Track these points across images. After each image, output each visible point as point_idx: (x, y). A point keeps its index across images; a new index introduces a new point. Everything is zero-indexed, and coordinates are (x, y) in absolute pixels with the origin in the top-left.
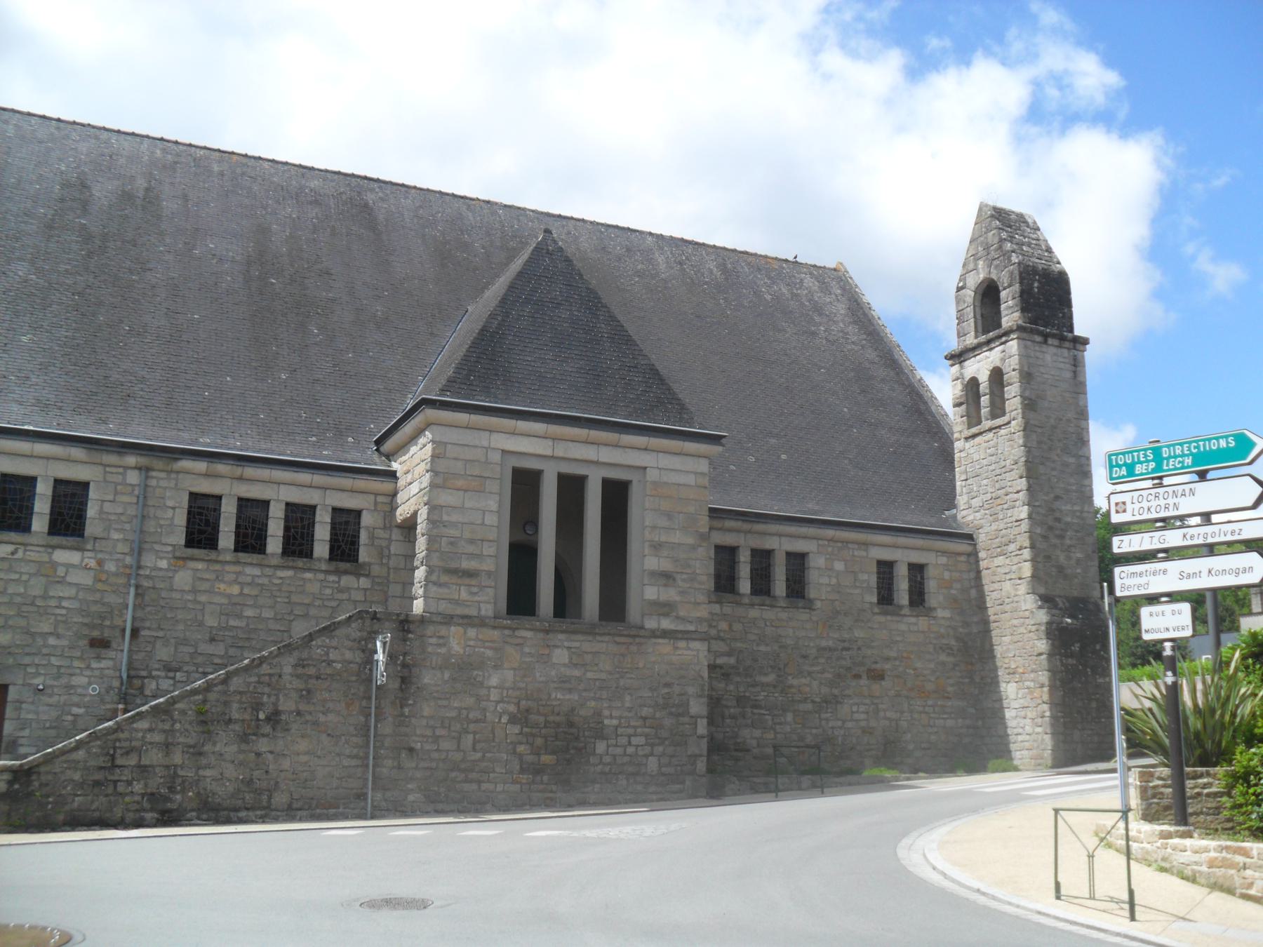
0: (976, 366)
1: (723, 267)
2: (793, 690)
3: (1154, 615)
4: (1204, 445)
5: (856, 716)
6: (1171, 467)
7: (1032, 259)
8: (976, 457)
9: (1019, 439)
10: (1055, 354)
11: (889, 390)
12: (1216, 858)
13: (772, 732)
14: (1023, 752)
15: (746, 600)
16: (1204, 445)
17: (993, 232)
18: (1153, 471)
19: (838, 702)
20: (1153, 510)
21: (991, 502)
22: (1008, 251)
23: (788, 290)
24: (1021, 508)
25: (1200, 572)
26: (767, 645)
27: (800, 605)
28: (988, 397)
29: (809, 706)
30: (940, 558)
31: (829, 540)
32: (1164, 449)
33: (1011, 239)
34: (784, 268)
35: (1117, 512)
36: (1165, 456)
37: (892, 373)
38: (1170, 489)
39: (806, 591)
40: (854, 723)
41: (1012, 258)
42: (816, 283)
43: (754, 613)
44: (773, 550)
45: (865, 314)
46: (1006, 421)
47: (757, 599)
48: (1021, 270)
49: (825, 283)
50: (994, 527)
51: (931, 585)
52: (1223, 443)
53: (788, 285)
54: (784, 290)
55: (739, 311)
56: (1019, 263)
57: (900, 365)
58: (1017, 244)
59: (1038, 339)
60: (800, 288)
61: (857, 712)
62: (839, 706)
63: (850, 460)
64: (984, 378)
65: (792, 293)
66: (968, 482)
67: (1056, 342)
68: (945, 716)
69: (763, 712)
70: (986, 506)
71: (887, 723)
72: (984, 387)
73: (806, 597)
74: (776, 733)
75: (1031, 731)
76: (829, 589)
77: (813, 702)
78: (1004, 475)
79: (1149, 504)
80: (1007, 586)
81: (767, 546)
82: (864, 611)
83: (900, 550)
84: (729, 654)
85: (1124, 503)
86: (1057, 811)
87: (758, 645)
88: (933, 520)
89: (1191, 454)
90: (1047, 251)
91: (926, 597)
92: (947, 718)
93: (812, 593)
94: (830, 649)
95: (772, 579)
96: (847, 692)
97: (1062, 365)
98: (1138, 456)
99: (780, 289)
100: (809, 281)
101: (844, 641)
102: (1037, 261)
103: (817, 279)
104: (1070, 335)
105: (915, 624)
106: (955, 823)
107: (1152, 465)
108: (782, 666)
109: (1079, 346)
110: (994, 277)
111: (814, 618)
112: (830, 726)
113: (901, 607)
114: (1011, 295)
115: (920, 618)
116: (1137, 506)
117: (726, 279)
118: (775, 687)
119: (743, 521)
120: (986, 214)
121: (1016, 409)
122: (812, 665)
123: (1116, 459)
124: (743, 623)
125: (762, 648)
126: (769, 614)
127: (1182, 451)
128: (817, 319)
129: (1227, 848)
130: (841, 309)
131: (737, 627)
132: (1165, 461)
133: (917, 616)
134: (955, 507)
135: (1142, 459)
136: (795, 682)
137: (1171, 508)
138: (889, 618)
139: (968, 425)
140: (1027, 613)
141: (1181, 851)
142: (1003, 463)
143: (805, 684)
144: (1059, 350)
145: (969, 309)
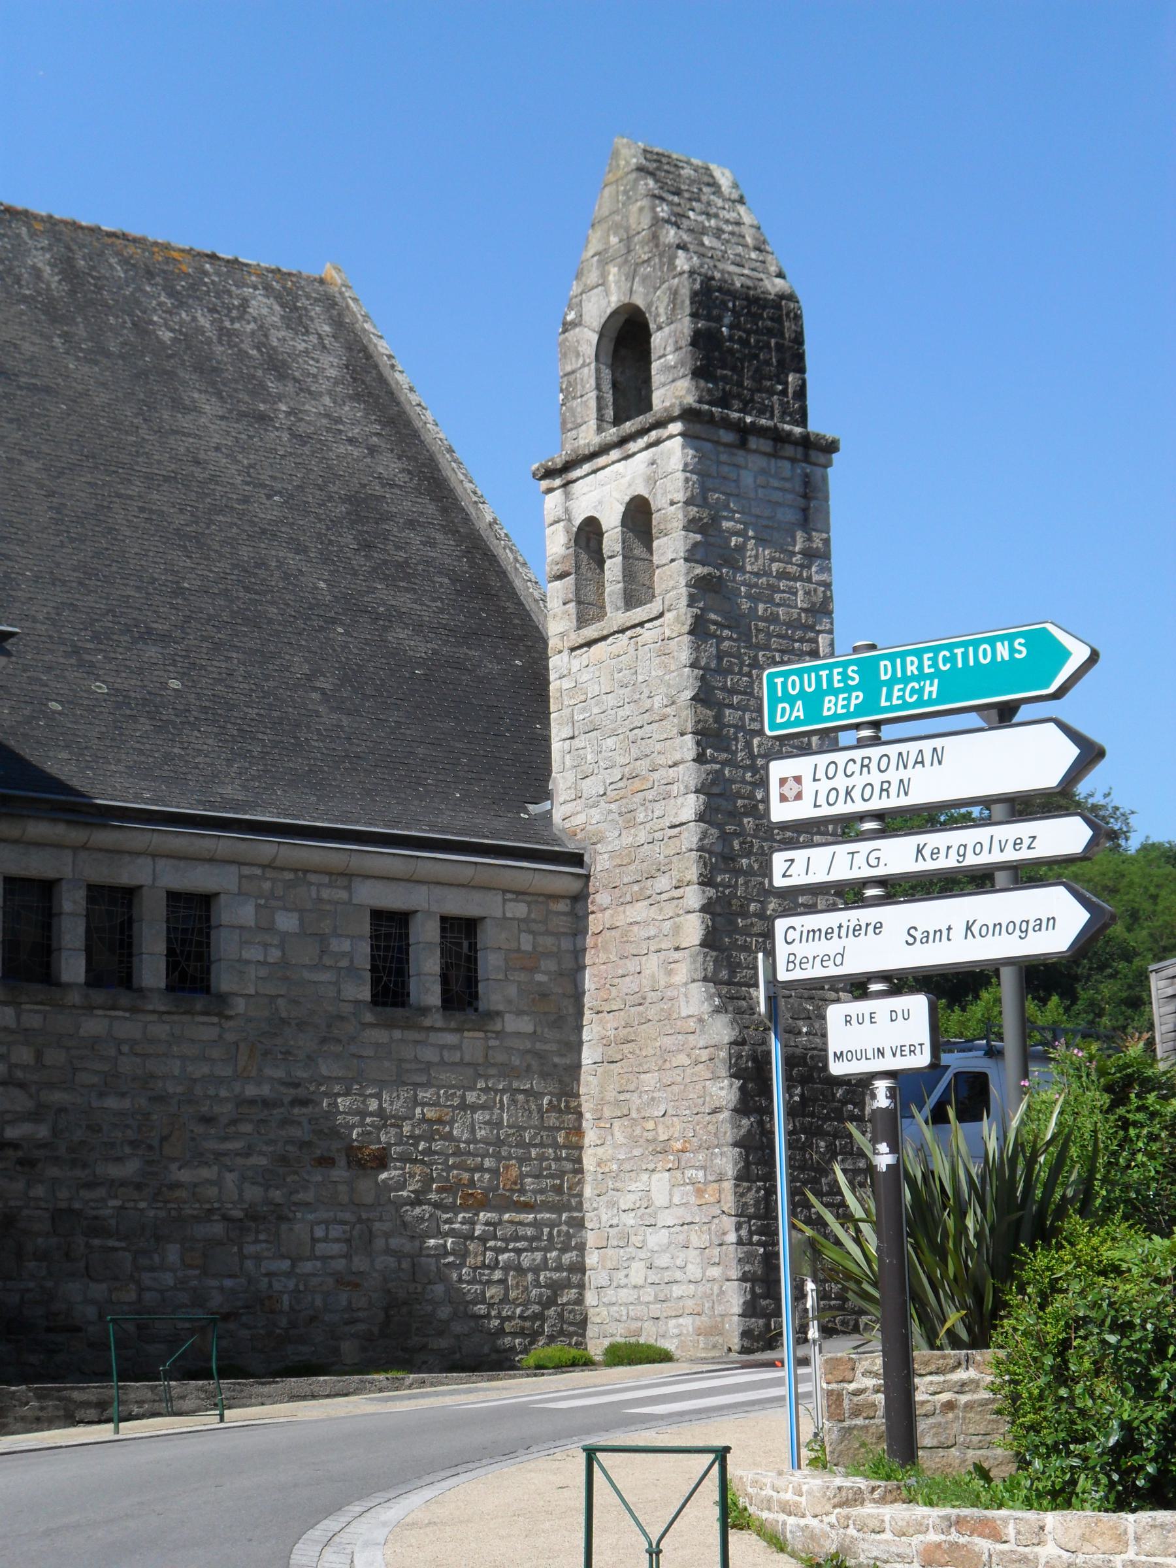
0: (595, 496)
1: (66, 267)
2: (182, 1194)
3: (854, 1022)
4: (965, 655)
5: (321, 1248)
6: (895, 702)
7: (720, 265)
8: (593, 690)
9: (682, 651)
10: (763, 472)
11: (424, 544)
12: (938, 1545)
13: (132, 1286)
14: (681, 1320)
15: (74, 997)
16: (965, 655)
17: (639, 204)
18: (860, 709)
19: (282, 1218)
20: (856, 794)
21: (620, 784)
22: (670, 246)
23: (212, 323)
24: (680, 800)
25: (949, 929)
26: (123, 1095)
27: (199, 1007)
28: (619, 559)
29: (217, 1229)
30: (510, 905)
31: (330, 874)
32: (882, 664)
33: (676, 221)
34: (206, 273)
35: (783, 798)
36: (883, 678)
37: (431, 509)
38: (893, 750)
39: (213, 975)
40: (318, 1264)
41: (678, 262)
42: (277, 308)
43: (93, 1026)
44: (141, 887)
45: (382, 380)
46: (655, 613)
47: (99, 996)
48: (697, 286)
49: (297, 308)
50: (627, 840)
51: (490, 963)
52: (1003, 651)
53: (213, 310)
54: (204, 321)
55: (96, 363)
56: (692, 273)
57: (452, 491)
58: (690, 231)
59: (727, 437)
60: (240, 318)
61: (326, 1240)
62: (284, 1227)
63: (323, 692)
64: (611, 520)
65: (221, 329)
66: (577, 743)
67: (766, 445)
68: (519, 1245)
69: (111, 1243)
70: (611, 795)
71: (391, 1261)
72: (612, 540)
73: (213, 989)
74: (141, 1289)
75: (699, 1276)
76: (263, 972)
77: (226, 1218)
78: (647, 727)
79: (850, 782)
80: (652, 964)
81: (472, 911)
82: (342, 1018)
83: (424, 889)
84: (35, 1116)
85: (798, 779)
86: (591, 1453)
87: (101, 1095)
88: (499, 824)
89: (938, 673)
90: (757, 249)
91: (481, 987)
92: (525, 1250)
93: (224, 981)
94: (266, 1103)
95: (135, 950)
96: (301, 1196)
97: (777, 496)
98: (830, 678)
99: (194, 319)
100: (261, 305)
101: (297, 1085)
102: (732, 268)
103: (278, 298)
104: (798, 430)
105: (458, 1047)
106: (445, 1484)
107: (858, 697)
108: (155, 1143)
109: (814, 455)
110: (640, 302)
111: (230, 1037)
112: (263, 1271)
113: (424, 1011)
114: (671, 341)
115: (466, 1034)
116: (824, 786)
117: (72, 292)
118: (139, 1187)
119: (69, 822)
120: (628, 163)
121: (674, 588)
122: (225, 1139)
123: (784, 684)
124: (68, 1049)
125: (112, 1103)
126: (128, 1028)
127: (920, 667)
128: (272, 386)
129: (959, 1522)
130: (330, 365)
131: (55, 1057)
132: (884, 690)
133: (459, 1030)
134: (547, 795)
135: (836, 685)
136: (185, 1176)
137: (893, 790)
138: (397, 1034)
139: (579, 619)
140: (692, 1024)
141: (873, 1531)
142: (647, 704)
143: (208, 1181)
144: (773, 461)
145: (586, 370)
